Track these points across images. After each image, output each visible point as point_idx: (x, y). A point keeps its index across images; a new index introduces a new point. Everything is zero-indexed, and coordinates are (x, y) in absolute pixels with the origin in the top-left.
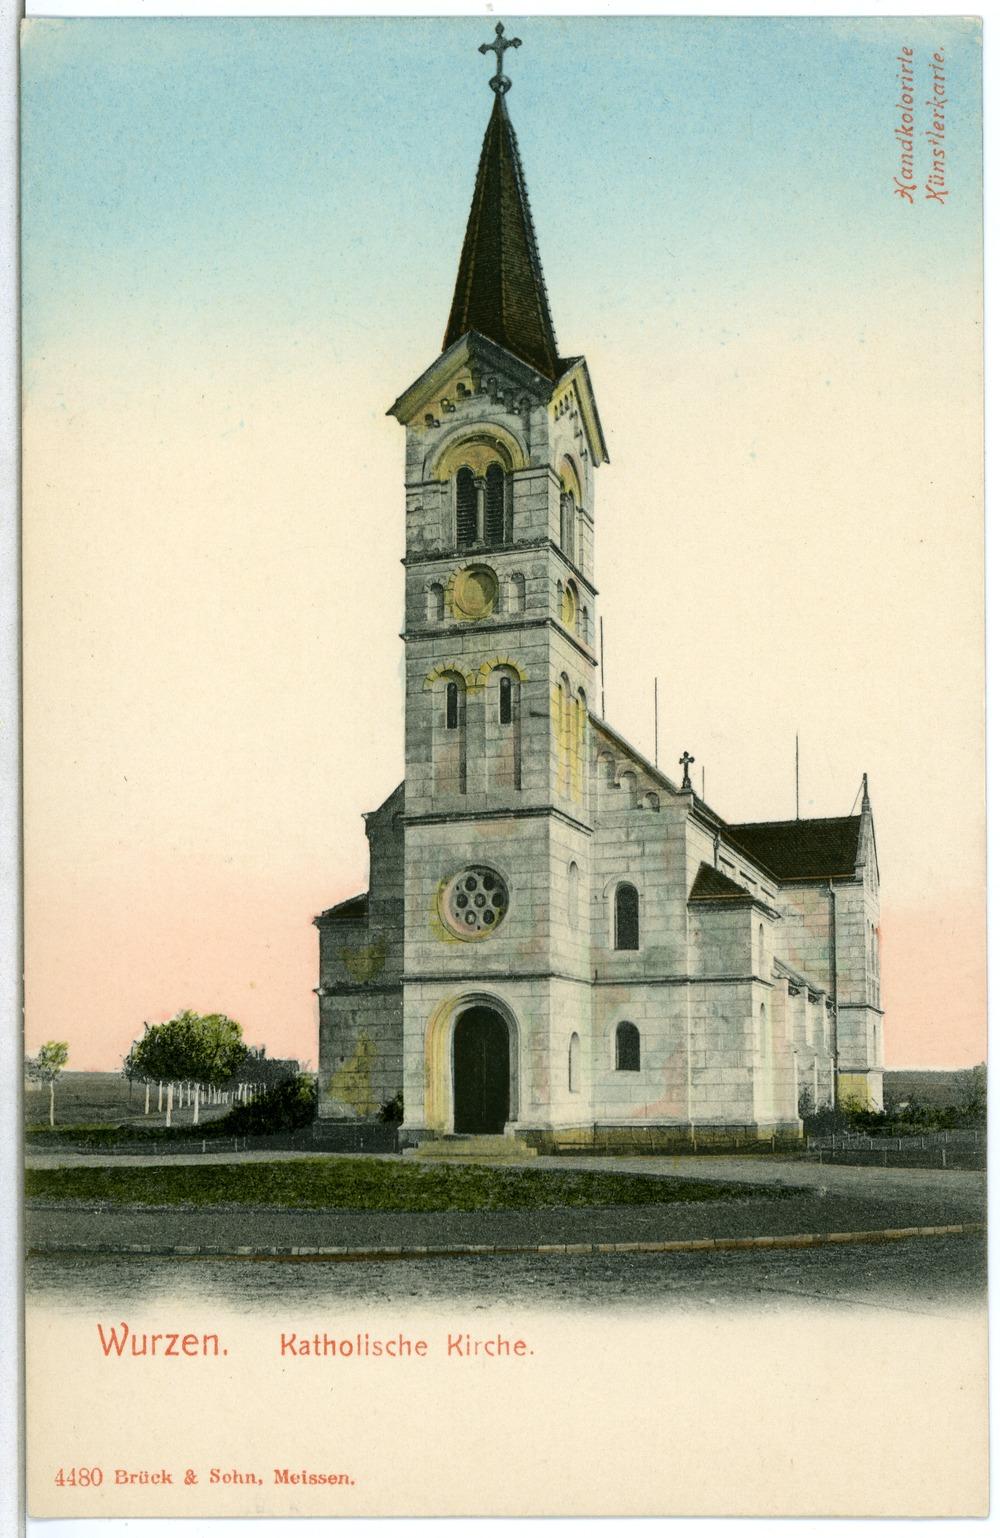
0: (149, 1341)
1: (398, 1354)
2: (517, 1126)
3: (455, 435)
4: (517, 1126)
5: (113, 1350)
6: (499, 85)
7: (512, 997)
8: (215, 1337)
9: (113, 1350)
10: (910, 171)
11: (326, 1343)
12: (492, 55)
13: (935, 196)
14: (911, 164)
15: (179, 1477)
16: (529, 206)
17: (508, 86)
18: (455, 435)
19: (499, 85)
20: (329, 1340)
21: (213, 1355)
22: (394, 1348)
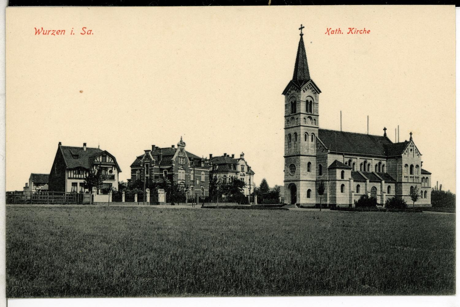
0: (48, 32)
1: (354, 33)
2: (296, 203)
3: (182, 181)
4: (296, 203)
5: (38, 33)
6: (301, 35)
7: (295, 183)
8: (64, 31)
9: (38, 33)
10: (333, 33)
11: (339, 31)
12: (301, 30)
13: (328, 31)
14: (338, 33)
15: (345, 30)
16: (412, 199)
17: (303, 35)
18: (182, 181)
19: (301, 35)
20: (340, 30)
21: (332, 29)
22: (361, 32)
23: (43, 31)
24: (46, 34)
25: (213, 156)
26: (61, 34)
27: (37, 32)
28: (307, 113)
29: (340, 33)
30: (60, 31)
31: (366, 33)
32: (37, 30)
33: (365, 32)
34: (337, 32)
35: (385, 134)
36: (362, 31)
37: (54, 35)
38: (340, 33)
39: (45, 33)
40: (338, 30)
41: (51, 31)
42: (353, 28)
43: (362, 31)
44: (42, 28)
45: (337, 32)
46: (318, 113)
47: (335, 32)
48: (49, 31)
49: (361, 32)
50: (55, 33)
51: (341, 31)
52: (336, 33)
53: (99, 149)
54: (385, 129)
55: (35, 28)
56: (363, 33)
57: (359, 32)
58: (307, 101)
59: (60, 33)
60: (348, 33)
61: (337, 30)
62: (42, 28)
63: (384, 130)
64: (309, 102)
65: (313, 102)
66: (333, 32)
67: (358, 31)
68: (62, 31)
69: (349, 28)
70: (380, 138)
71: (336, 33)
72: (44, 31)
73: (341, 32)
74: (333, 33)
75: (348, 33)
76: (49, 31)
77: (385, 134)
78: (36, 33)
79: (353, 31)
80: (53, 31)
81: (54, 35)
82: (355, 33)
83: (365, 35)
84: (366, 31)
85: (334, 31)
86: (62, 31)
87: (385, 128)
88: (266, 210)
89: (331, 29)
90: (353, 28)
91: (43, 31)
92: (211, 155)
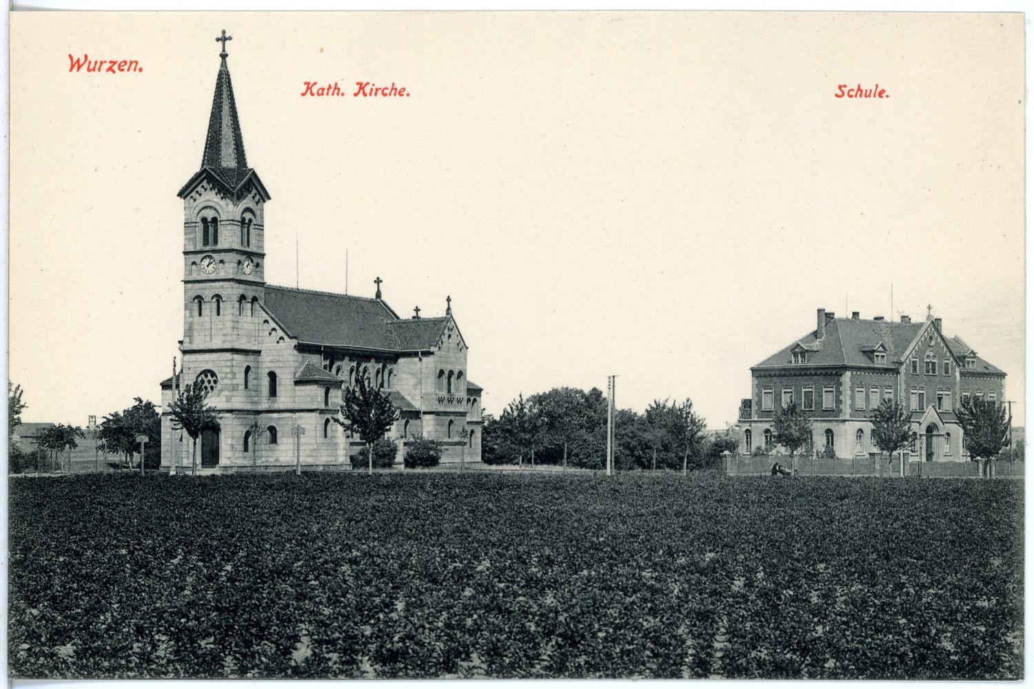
10: (322, 94)
11: (335, 88)
15: (349, 87)
23: (87, 63)
24: (94, 69)
25: (862, 317)
26: (129, 70)
27: (75, 65)
28: (243, 249)
29: (338, 94)
30: (126, 62)
31: (395, 95)
32: (75, 60)
33: (394, 91)
34: (331, 91)
35: (378, 295)
36: (387, 89)
37: (114, 72)
38: (338, 94)
39: (91, 67)
40: (333, 86)
41: (105, 62)
42: (368, 84)
43: (387, 89)
44: (86, 57)
45: (331, 91)
46: (262, 247)
47: (325, 91)
48: (101, 63)
49: (386, 91)
50: (115, 68)
51: (339, 89)
52: (327, 94)
53: (377, 305)
54: (378, 281)
55: (71, 57)
56: (390, 94)
57: (379, 92)
58: (204, 220)
59: (126, 68)
60: (356, 95)
61: (330, 87)
62: (86, 57)
63: (375, 282)
64: (209, 220)
65: (219, 219)
66: (321, 92)
67: (377, 90)
68: (131, 63)
69: (305, 83)
70: (371, 301)
71: (327, 94)
72: (90, 62)
73: (340, 93)
74: (322, 94)
75: (356, 95)
76: (101, 63)
77: (378, 295)
78: (72, 67)
79: (367, 90)
80: (111, 62)
81: (114, 72)
82: (370, 95)
83: (393, 99)
84: (396, 89)
85: (323, 89)
86: (131, 63)
87: (378, 278)
88: (82, 472)
89: (315, 83)
90: (368, 84)
91: (87, 63)
92: (855, 314)
